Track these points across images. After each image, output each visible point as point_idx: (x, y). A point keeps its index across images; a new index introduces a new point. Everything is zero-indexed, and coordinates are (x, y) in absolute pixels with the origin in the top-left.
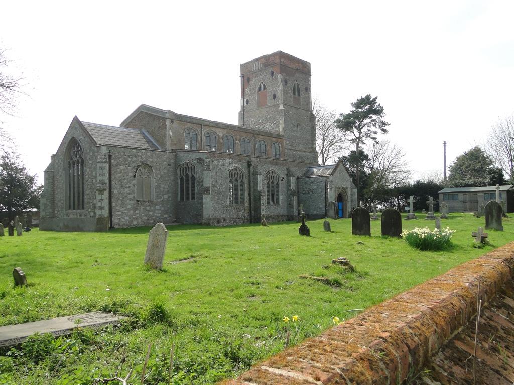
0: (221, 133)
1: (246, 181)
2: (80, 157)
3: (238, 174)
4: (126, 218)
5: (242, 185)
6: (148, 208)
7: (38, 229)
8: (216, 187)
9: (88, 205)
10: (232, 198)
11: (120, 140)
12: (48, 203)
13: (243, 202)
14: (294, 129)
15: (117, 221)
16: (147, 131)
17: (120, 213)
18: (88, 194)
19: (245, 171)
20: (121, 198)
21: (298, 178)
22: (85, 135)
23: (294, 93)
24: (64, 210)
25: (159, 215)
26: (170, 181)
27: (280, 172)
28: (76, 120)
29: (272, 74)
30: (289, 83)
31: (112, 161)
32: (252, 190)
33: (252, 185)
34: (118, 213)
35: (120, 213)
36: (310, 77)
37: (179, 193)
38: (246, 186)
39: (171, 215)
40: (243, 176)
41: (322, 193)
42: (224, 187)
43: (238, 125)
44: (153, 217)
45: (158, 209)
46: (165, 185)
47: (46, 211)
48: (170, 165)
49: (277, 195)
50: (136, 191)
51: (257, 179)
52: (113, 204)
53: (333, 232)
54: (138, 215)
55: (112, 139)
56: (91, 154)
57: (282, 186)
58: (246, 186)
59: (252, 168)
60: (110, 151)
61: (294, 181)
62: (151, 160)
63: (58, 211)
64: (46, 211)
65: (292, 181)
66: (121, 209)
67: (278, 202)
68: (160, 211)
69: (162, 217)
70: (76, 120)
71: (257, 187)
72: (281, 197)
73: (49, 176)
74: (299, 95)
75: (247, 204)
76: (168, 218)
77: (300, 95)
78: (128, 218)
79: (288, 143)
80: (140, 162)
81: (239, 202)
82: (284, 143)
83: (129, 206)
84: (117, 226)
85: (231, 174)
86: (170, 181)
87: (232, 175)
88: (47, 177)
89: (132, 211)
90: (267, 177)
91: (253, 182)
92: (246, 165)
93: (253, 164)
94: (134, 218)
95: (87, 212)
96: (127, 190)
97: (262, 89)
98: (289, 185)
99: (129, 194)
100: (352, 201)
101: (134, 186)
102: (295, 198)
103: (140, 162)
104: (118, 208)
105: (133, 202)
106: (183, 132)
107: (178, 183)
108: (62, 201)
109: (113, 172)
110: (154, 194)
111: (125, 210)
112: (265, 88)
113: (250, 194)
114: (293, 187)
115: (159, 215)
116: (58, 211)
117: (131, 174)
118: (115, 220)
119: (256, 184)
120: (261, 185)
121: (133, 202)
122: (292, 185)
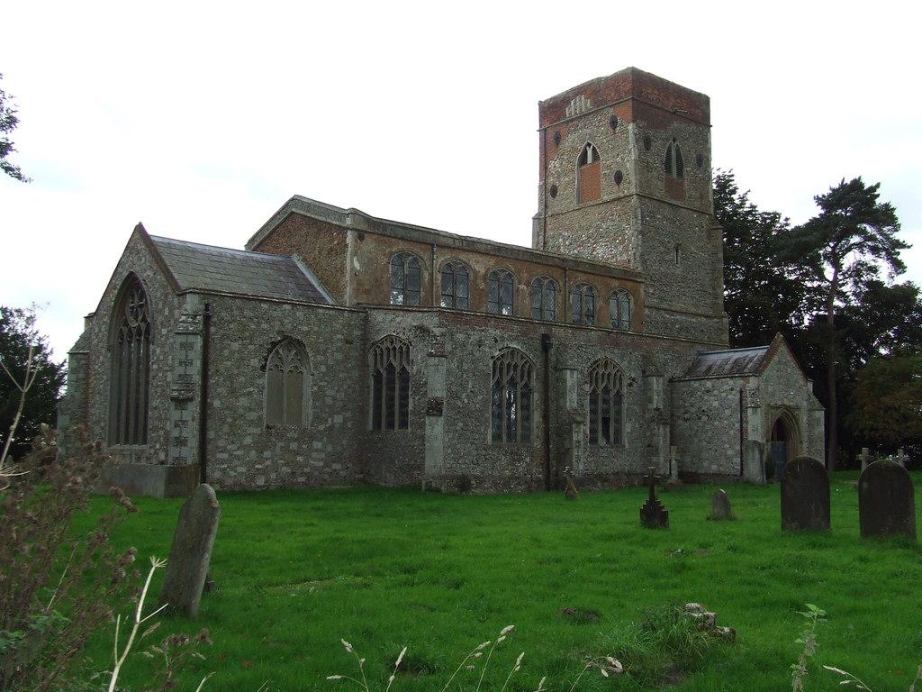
2: (144, 320)
11: (236, 279)
13: (526, 437)
17: (225, 456)
18: (155, 408)
29: (614, 123)
31: (212, 329)
32: (553, 407)
34: (220, 456)
35: (225, 456)
36: (709, 132)
42: (480, 397)
45: (316, 450)
49: (618, 421)
50: (265, 405)
52: (211, 434)
54: (268, 463)
62: (305, 328)
66: (229, 447)
68: (323, 455)
70: (140, 229)
76: (343, 473)
78: (242, 469)
80: (278, 333)
83: (248, 441)
89: (253, 453)
92: (537, 344)
93: (554, 341)
96: (243, 401)
97: (590, 160)
101: (261, 392)
103: (278, 333)
104: (221, 443)
105: (257, 431)
109: (212, 356)
110: (310, 411)
112: (596, 157)
114: (657, 401)
117: (255, 362)
120: (575, 396)
121: (257, 431)
122: (655, 397)
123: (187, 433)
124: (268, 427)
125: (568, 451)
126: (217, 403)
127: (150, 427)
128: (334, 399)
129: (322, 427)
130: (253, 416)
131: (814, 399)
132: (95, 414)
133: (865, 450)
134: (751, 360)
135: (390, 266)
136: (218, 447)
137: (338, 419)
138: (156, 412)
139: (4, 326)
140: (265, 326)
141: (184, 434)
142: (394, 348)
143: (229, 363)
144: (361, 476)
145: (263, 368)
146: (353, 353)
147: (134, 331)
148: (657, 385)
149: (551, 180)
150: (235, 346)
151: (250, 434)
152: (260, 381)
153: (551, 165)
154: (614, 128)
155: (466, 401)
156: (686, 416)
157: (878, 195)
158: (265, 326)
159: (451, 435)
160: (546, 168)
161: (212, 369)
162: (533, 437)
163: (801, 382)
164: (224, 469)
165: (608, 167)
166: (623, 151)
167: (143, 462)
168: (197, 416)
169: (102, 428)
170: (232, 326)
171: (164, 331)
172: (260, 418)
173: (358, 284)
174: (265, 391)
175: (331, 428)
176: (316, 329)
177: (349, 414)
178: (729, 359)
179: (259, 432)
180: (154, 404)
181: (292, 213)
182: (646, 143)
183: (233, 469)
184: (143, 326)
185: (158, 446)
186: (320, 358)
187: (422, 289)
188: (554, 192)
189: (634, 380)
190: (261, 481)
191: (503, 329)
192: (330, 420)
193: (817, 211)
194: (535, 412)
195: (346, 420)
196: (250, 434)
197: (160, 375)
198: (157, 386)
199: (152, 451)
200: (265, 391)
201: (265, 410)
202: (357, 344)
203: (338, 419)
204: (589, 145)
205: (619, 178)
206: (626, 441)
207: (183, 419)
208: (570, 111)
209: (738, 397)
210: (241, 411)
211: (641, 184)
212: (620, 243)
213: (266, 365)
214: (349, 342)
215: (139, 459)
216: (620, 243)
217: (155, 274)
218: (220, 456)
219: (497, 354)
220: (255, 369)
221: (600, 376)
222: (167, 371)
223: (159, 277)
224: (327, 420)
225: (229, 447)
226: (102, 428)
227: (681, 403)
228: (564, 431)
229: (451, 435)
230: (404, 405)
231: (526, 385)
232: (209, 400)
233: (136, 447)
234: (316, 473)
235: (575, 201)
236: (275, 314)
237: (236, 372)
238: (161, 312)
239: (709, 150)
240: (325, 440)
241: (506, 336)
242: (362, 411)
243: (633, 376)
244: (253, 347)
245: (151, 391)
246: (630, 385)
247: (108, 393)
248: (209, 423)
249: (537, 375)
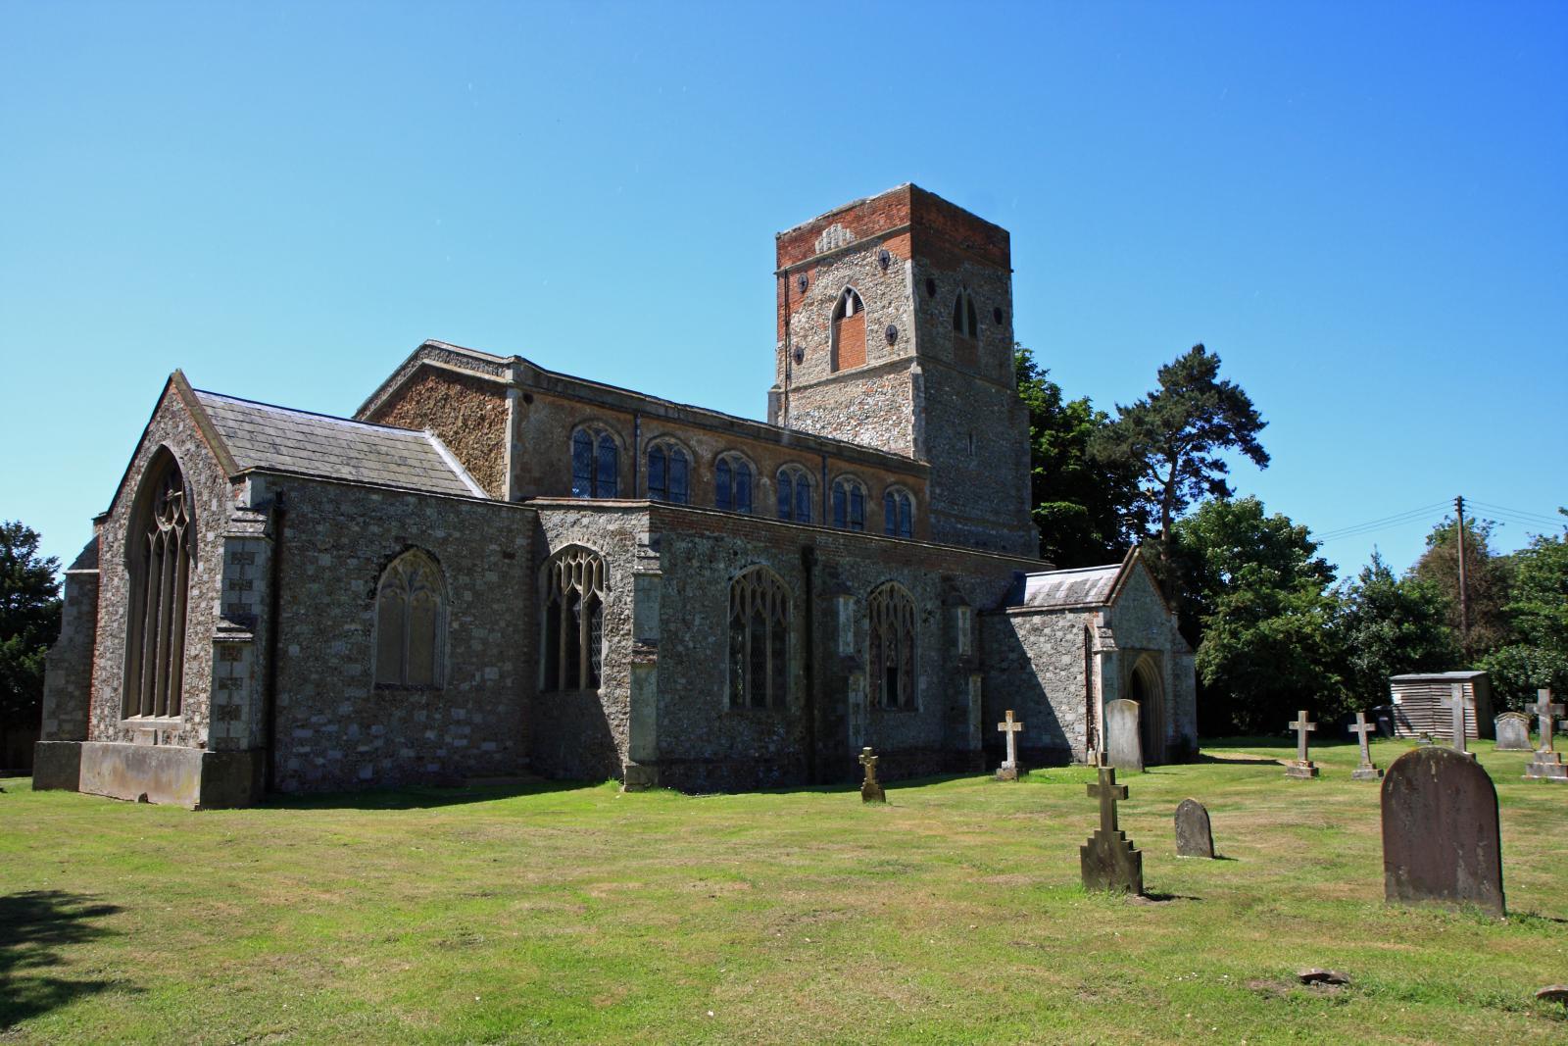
0: (705, 446)
1: (794, 617)
2: (181, 521)
3: (763, 595)
4: (331, 754)
5: (780, 635)
6: (421, 716)
7: (29, 781)
8: (682, 641)
9: (191, 701)
10: (633, 884)
11: (333, 459)
12: (71, 688)
13: (780, 702)
14: (959, 445)
15: (293, 764)
16: (439, 436)
17: (307, 733)
18: (196, 657)
19: (794, 592)
20: (314, 676)
21: (980, 614)
22: (199, 435)
23: (958, 326)
24: (119, 716)
25: (465, 742)
26: (508, 617)
27: (913, 590)
28: (176, 382)
29: (885, 262)
30: (942, 289)
31: (288, 533)
32: (818, 652)
33: (817, 635)
34: (299, 733)
35: (307, 733)
36: (1010, 278)
37: (543, 662)
38: (794, 639)
39: (509, 744)
40: (784, 602)
41: (1074, 670)
42: (711, 639)
43: (765, 420)
44: (441, 752)
45: (458, 722)
46: (492, 630)
47: (63, 717)
48: (511, 556)
49: (910, 673)
50: (374, 651)
51: (835, 614)
52: (284, 699)
53: (1221, 858)
54: (379, 743)
55: (304, 454)
56: (214, 507)
57: (926, 648)
58: (794, 639)
59: (817, 571)
60: (279, 495)
61: (968, 625)
62: (440, 534)
63: (102, 719)
64: (63, 717)
65: (960, 623)
66: (314, 719)
67: (910, 705)
68: (467, 730)
69: (475, 751)
70: (176, 382)
71: (836, 642)
72: (922, 684)
73: (81, 588)
74: (973, 332)
75: (795, 710)
76: (497, 756)
77: (978, 331)
78: (338, 754)
79: (938, 491)
80: (397, 539)
81: (769, 699)
82: (928, 492)
83: (345, 709)
84: (292, 785)
85: (737, 597)
86: (508, 617)
87: (743, 597)
88: (75, 593)
89: (354, 728)
90: (873, 612)
91: (818, 627)
92: (795, 558)
93: (820, 556)
94: (362, 754)
95: (188, 726)
96: (339, 646)
97: (849, 310)
98: (948, 639)
99: (350, 659)
100: (1177, 695)
101: (367, 633)
102: (974, 683)
103: (397, 539)
104: (300, 714)
105: (361, 693)
106: (569, 438)
107: (539, 624)
108: (115, 684)
109: (288, 574)
110: (447, 662)
111: (330, 722)
112: (857, 302)
113: (808, 668)
114: (964, 645)
115: (465, 742)
116: (102, 719)
117: (359, 586)
118: (289, 763)
119: (832, 634)
120: (850, 637)
121: (361, 693)
122: (961, 638)
123: (242, 698)
124: (378, 687)
125: (842, 720)
126: (294, 650)
127: (185, 687)
128: (484, 642)
129: (465, 686)
130: (356, 669)
131: (1179, 636)
132: (104, 669)
133: (1302, 714)
134: (1094, 585)
135: (572, 443)
136: (295, 720)
137: (491, 673)
138: (195, 664)
139: (1301, 725)
140: (375, 529)
141: (236, 700)
142: (579, 565)
143: (315, 587)
144: (528, 760)
145: (372, 594)
146: (518, 572)
147: (166, 539)
148: (963, 618)
149: (794, 340)
150: (326, 560)
151: (348, 699)
152: (367, 615)
153: (794, 320)
154: (885, 268)
155: (691, 645)
156: (1004, 665)
157: (1151, 396)
158: (375, 529)
159: (668, 698)
160: (787, 324)
161: (286, 596)
162: (789, 698)
163: (1164, 617)
164: (306, 755)
165: (878, 321)
166: (893, 299)
167: (174, 745)
168: (259, 670)
169: (116, 690)
170: (320, 528)
171: (211, 536)
172: (366, 673)
173: (522, 469)
174: (374, 634)
175: (480, 688)
176: (603, 920)
177: (508, 666)
178: (1060, 585)
179: (365, 696)
180: (193, 653)
181: (424, 365)
182: (926, 287)
183: (323, 753)
184: (180, 531)
185: (197, 719)
186: (463, 579)
187: (619, 479)
188: (799, 357)
189: (930, 613)
190: (367, 773)
191: (746, 536)
192: (478, 677)
193: (1157, 387)
194: (793, 662)
195: (502, 676)
196: (348, 699)
197: (203, 605)
198: (199, 623)
199: (188, 726)
200: (374, 634)
201: (374, 661)
202: (522, 558)
203: (491, 673)
204: (849, 291)
205: (892, 336)
206: (920, 703)
207: (235, 675)
208: (823, 244)
209: (1082, 637)
210: (334, 662)
211: (920, 346)
212: (895, 425)
213: (376, 589)
214: (511, 556)
215: (167, 739)
216: (895, 425)
217: (198, 447)
218: (299, 733)
219: (738, 574)
220: (357, 596)
221: (883, 609)
222: (212, 599)
223: (204, 452)
224: (474, 676)
225: (314, 719)
226: (116, 690)
227: (995, 646)
228: (837, 690)
229: (668, 698)
230: (593, 651)
231: (779, 623)
232: (280, 645)
233: (165, 719)
234: (457, 757)
235: (829, 368)
236: (392, 510)
237: (326, 600)
238: (206, 506)
239: (1010, 304)
240: (470, 706)
241: (749, 546)
242: (531, 662)
243: (929, 607)
244: (355, 561)
245: (189, 630)
246: (925, 621)
247: (124, 635)
248: (283, 681)
249: (796, 607)
